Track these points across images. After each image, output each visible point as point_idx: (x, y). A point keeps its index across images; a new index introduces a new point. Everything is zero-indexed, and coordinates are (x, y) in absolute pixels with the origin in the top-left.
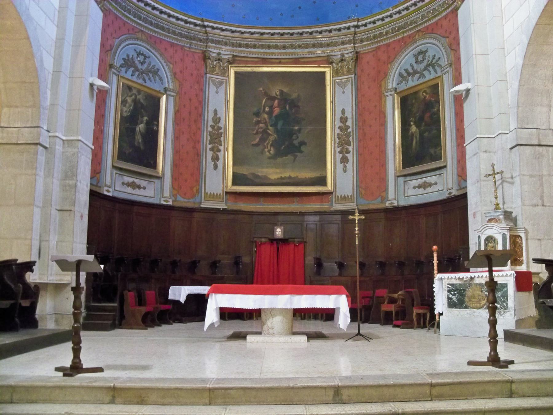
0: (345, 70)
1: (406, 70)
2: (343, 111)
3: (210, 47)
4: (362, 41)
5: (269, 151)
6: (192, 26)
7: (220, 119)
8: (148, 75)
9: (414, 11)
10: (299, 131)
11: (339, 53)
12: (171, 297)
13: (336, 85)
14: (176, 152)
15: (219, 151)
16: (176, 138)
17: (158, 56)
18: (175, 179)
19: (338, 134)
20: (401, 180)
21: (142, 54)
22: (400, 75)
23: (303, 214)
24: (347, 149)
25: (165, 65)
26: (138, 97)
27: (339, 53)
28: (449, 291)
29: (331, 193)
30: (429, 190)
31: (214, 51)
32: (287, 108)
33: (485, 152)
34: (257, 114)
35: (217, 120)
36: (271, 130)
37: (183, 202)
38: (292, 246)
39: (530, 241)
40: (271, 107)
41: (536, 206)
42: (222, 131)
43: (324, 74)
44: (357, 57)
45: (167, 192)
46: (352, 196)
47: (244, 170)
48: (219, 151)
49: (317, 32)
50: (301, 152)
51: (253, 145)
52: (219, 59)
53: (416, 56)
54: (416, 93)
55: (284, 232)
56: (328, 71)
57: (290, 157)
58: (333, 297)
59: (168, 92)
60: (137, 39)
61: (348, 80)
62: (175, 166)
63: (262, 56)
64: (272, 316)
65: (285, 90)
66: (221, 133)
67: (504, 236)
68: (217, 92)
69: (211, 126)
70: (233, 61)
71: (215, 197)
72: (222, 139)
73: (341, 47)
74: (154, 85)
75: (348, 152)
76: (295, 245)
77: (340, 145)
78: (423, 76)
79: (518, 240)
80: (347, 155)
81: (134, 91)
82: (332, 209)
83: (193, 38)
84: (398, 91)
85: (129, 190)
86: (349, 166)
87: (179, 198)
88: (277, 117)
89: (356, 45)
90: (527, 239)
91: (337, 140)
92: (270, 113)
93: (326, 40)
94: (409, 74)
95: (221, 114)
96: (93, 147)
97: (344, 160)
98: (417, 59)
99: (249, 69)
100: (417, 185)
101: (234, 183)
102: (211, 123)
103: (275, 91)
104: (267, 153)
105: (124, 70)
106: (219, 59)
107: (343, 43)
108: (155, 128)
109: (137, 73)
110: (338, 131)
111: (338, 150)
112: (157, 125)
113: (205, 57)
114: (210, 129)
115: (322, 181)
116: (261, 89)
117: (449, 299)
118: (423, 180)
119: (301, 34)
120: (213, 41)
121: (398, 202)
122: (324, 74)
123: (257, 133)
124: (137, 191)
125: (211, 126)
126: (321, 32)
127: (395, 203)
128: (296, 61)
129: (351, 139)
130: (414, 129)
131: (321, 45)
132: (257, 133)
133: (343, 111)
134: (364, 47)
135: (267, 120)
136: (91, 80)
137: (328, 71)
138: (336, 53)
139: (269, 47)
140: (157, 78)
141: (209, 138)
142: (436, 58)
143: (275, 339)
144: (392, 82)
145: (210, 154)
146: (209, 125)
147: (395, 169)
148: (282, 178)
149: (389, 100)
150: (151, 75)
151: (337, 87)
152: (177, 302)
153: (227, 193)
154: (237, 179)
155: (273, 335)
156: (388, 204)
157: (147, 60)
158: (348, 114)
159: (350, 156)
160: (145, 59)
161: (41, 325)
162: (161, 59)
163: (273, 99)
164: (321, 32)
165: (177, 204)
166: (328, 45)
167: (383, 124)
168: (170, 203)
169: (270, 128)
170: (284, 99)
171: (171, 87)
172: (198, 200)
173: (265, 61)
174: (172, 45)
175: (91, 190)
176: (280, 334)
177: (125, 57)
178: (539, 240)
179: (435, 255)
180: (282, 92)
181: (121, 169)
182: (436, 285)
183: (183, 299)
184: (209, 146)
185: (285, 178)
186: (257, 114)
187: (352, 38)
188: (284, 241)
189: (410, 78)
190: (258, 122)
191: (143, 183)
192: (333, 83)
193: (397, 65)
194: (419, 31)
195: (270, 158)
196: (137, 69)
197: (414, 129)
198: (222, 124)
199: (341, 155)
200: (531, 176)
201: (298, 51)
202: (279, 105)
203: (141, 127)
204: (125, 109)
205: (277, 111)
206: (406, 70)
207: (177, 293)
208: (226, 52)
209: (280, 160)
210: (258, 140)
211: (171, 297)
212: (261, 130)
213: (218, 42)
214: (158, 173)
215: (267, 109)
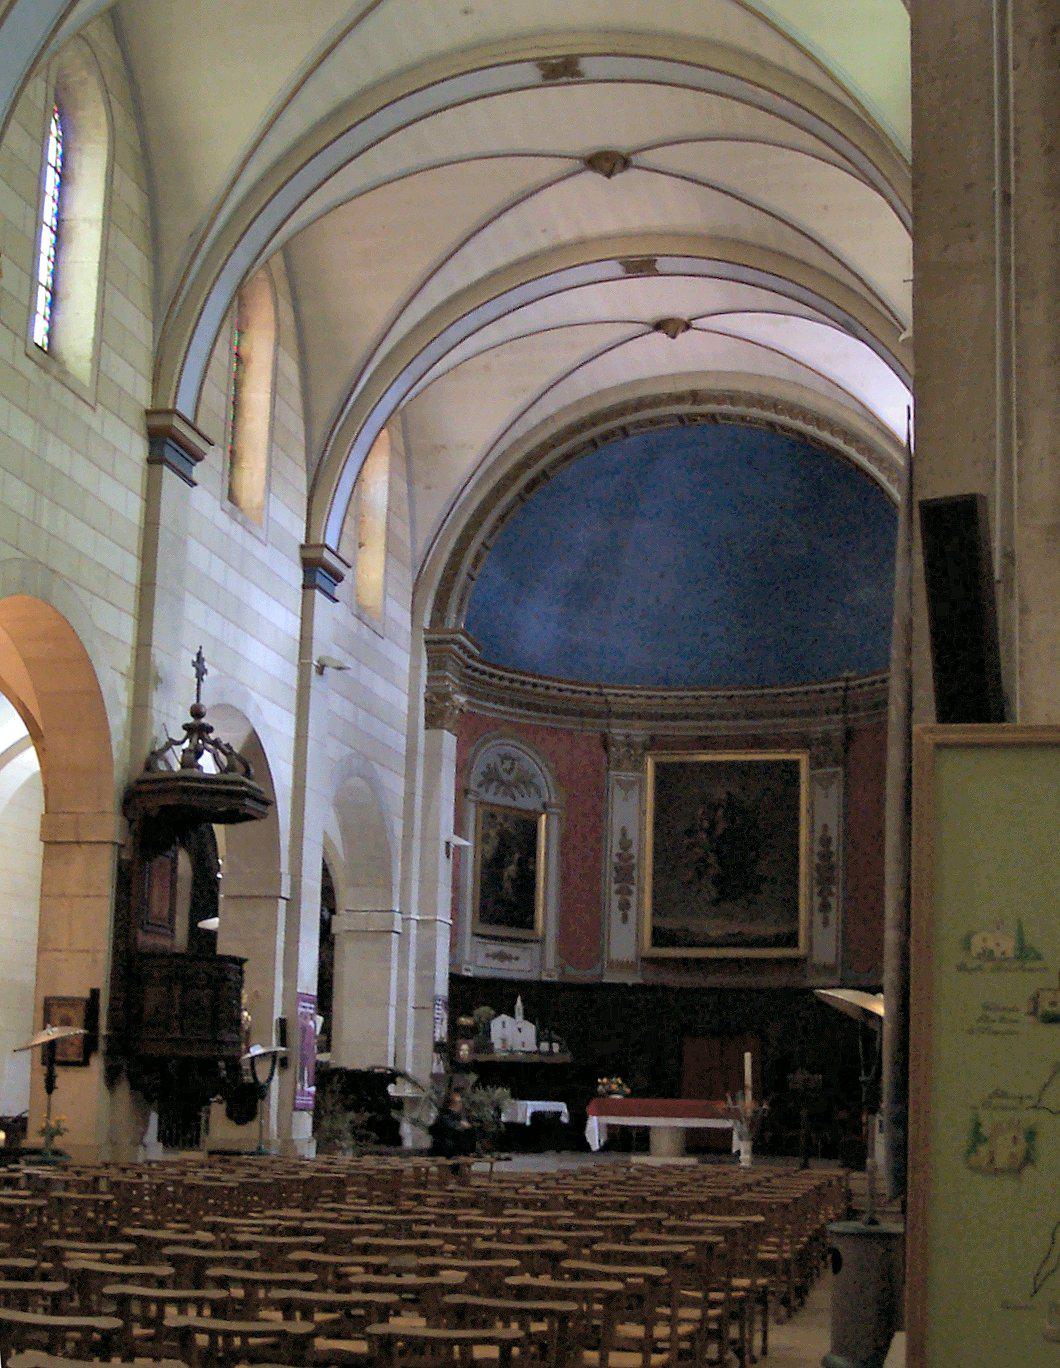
2: (825, 827)
15: (630, 892)
18: (564, 936)
31: (618, 732)
35: (625, 844)
36: (712, 859)
40: (713, 825)
42: (634, 861)
43: (796, 763)
44: (849, 735)
45: (551, 960)
47: (669, 923)
56: (803, 758)
61: (834, 775)
62: (563, 924)
68: (625, 799)
69: (617, 855)
71: (623, 966)
81: (500, 819)
85: (496, 963)
86: (833, 916)
95: (632, 834)
96: (451, 922)
97: (825, 907)
102: (616, 849)
103: (719, 793)
105: (483, 789)
108: (531, 867)
110: (816, 860)
111: (816, 890)
113: (606, 743)
114: (616, 860)
115: (791, 940)
122: (796, 763)
124: (506, 964)
125: (617, 855)
133: (825, 827)
137: (803, 758)
145: (616, 899)
153: (644, 959)
154: (660, 937)
158: (834, 833)
159: (832, 901)
160: (513, 764)
168: (556, 979)
172: (598, 971)
173: (705, 743)
175: (450, 974)
181: (483, 936)
184: (615, 887)
192: (812, 779)
196: (502, 783)
198: (634, 850)
203: (511, 870)
204: (487, 848)
208: (639, 732)
209: (727, 906)
215: (706, 824)
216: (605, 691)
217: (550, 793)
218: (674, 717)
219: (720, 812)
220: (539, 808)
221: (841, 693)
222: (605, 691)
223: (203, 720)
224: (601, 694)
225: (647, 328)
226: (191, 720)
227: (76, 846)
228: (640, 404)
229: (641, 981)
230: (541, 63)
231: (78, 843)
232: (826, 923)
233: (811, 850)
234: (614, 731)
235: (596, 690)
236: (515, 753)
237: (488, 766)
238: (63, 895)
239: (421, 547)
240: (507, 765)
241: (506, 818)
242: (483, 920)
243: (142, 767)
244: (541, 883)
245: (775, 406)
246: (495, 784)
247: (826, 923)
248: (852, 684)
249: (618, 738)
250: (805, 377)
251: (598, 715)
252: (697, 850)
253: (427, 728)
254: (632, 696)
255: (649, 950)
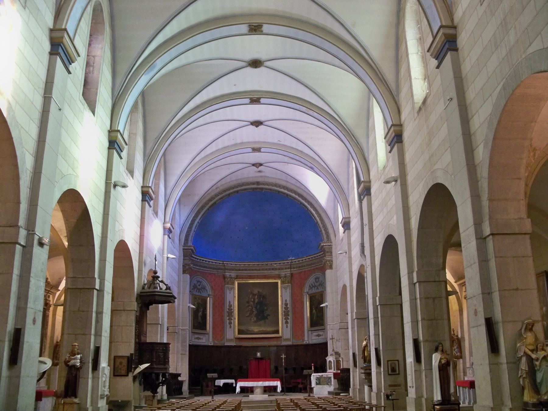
0: (287, 282)
1: (312, 284)
2: (286, 301)
3: (226, 272)
4: (294, 268)
5: (254, 319)
6: (218, 264)
7: (232, 305)
8: (201, 290)
9: (314, 259)
10: (267, 310)
11: (284, 273)
12: (216, 384)
13: (283, 288)
14: (214, 322)
15: (232, 320)
16: (214, 315)
17: (205, 280)
18: (213, 333)
19: (284, 311)
20: (310, 332)
21: (199, 282)
22: (310, 286)
23: (269, 346)
24: (288, 318)
25: (208, 284)
26: (199, 301)
27: (284, 273)
28: (316, 379)
29: (281, 337)
30: (320, 337)
31: (227, 274)
32: (261, 299)
33: (332, 329)
34: (248, 302)
35: (230, 306)
36: (254, 310)
37: (218, 343)
38: (264, 361)
39: (344, 362)
40: (254, 299)
41: (346, 349)
43: (277, 283)
44: (292, 275)
46: (290, 339)
47: (243, 328)
48: (232, 320)
49: (274, 264)
50: (268, 319)
51: (247, 316)
52: (231, 278)
53: (316, 279)
54: (315, 296)
55: (261, 355)
56: (279, 282)
57: (263, 321)
58: (276, 382)
59: (210, 296)
60: (197, 276)
61: (288, 286)
63: (250, 274)
64: (257, 389)
65: (261, 291)
66: (232, 312)
67: (334, 361)
70: (237, 277)
71: (231, 340)
72: (233, 314)
73: (285, 270)
74: (204, 294)
75: (288, 319)
76: (266, 360)
77: (285, 315)
78: (318, 288)
79: (339, 362)
80: (288, 320)
82: (282, 344)
83: (219, 269)
84: (309, 293)
85: (197, 340)
86: (289, 325)
87: (216, 342)
88: (257, 303)
89: (292, 270)
90: (343, 361)
91: (284, 314)
92: (254, 302)
93: (278, 267)
94: (313, 286)
97: (287, 322)
98: (316, 280)
99: (244, 281)
100: (316, 335)
101: (239, 333)
102: (228, 307)
103: (256, 291)
104: (253, 320)
106: (231, 278)
107: (286, 269)
109: (198, 290)
110: (284, 309)
111: (284, 318)
112: (206, 311)
113: (224, 277)
114: (228, 310)
115: (277, 332)
116: (250, 291)
117: (316, 382)
118: (318, 333)
119: (267, 264)
120: (227, 269)
121: (309, 341)
123: (248, 311)
126: (276, 264)
127: (308, 342)
128: (265, 277)
129: (289, 313)
130: (314, 311)
131: (276, 269)
132: (248, 311)
133: (286, 301)
134: (295, 271)
135: (253, 305)
136: (189, 305)
138: (283, 273)
139: (253, 270)
140: (205, 290)
141: (227, 314)
142: (323, 282)
143: (258, 396)
144: (306, 289)
145: (228, 321)
146: (233, 320)
147: (308, 327)
148: (259, 331)
149: (305, 297)
150: (203, 290)
151: (283, 290)
152: (219, 386)
153: (236, 338)
154: (240, 332)
155: (258, 394)
156: (305, 343)
157: (201, 283)
158: (288, 302)
159: (289, 321)
161: (184, 394)
162: (206, 281)
163: (254, 295)
164: (276, 264)
165: (215, 345)
166: (279, 269)
167: (303, 307)
168: (212, 344)
169: (254, 308)
170: (260, 295)
171: (211, 294)
173: (251, 277)
174: (210, 274)
176: (260, 394)
177: (193, 285)
178: (347, 361)
179: (313, 367)
180: (259, 292)
182: (312, 378)
183: (221, 385)
184: (228, 318)
185: (261, 331)
186: (248, 302)
187: (289, 267)
188: (261, 359)
189: (313, 288)
190: (249, 306)
191: (201, 337)
193: (308, 281)
194: (316, 268)
195: (254, 322)
196: (198, 289)
197: (314, 311)
199: (285, 320)
200: (344, 339)
201: (266, 271)
202: (257, 298)
205: (256, 301)
206: (312, 284)
207: (219, 382)
208: (233, 274)
210: (248, 314)
211: (216, 384)
212: (250, 309)
213: (230, 270)
214: (207, 332)
215: (252, 300)
216: (224, 263)
217: (210, 292)
218: (242, 270)
219: (256, 297)
220: (207, 296)
221: (290, 263)
222: (224, 263)
223: (157, 275)
224: (223, 264)
225: (251, 165)
226: (153, 275)
227: (123, 312)
228: (243, 185)
229: (235, 345)
230: (251, 99)
231: (124, 310)
232: (287, 327)
233: (282, 307)
234: (227, 274)
235: (222, 262)
236: (201, 280)
237: (194, 284)
238: (119, 326)
239: (182, 222)
240: (199, 284)
241: (199, 299)
242: (194, 328)
243: (141, 288)
244: (208, 318)
245: (280, 186)
246: (196, 289)
247: (287, 327)
248: (293, 261)
249: (227, 276)
250: (289, 180)
251: (222, 269)
252: (250, 307)
253: (183, 274)
254: (231, 264)
255: (237, 335)
